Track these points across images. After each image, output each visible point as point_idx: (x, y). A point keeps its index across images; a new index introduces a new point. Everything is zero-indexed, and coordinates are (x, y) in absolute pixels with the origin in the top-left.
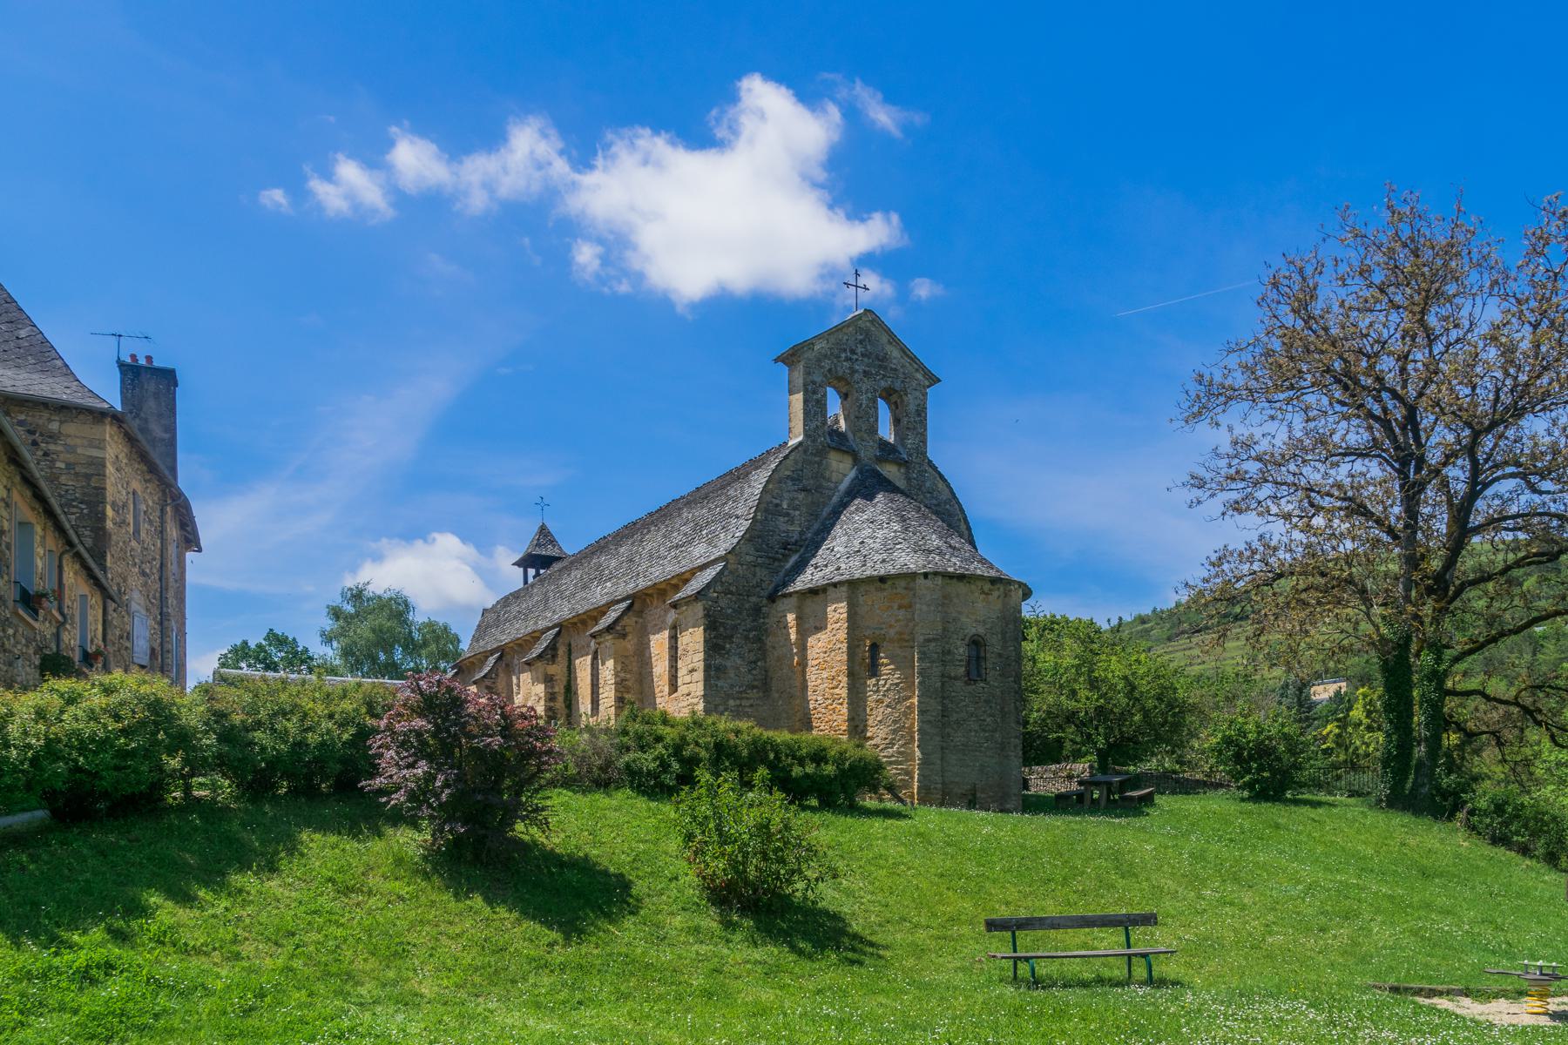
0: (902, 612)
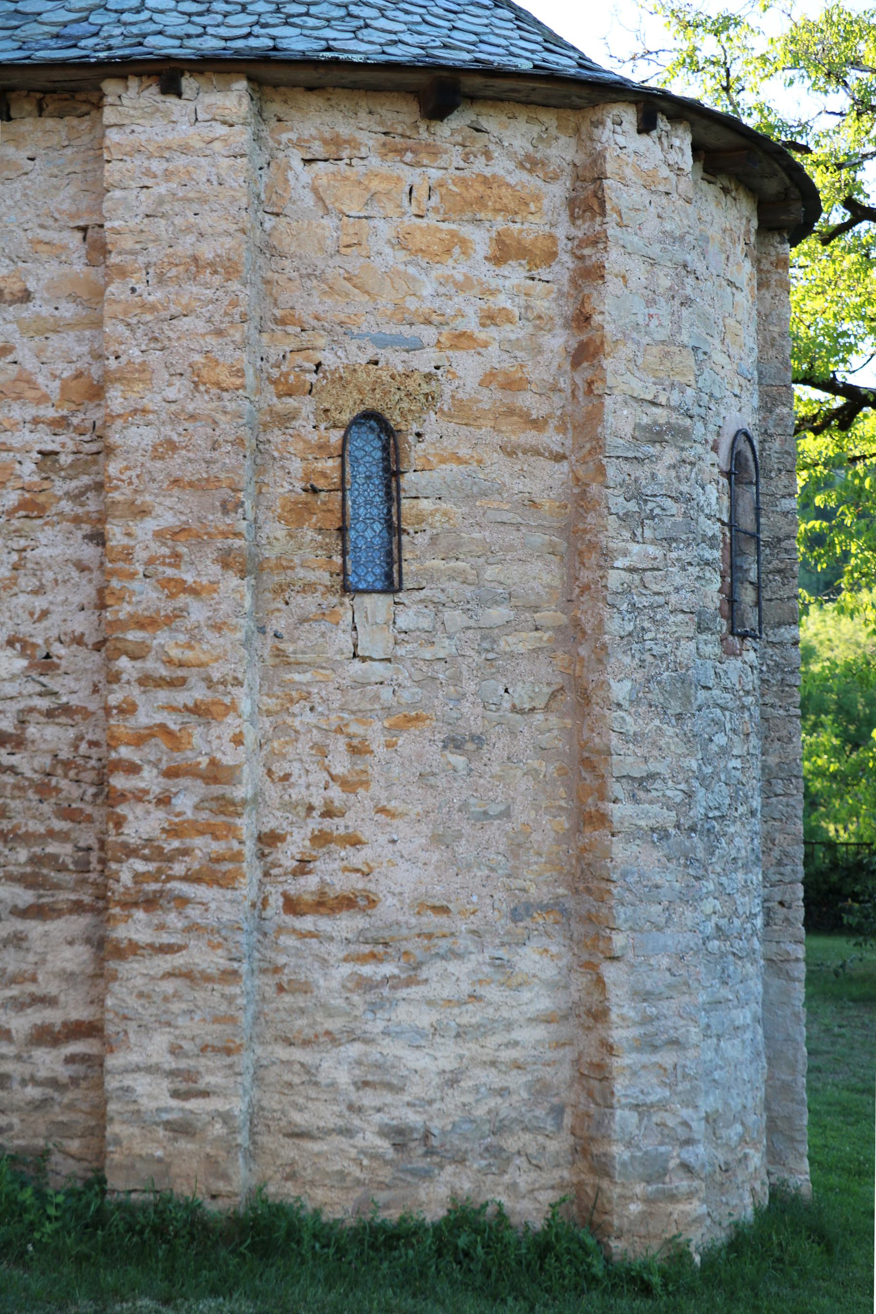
0: (514, 274)
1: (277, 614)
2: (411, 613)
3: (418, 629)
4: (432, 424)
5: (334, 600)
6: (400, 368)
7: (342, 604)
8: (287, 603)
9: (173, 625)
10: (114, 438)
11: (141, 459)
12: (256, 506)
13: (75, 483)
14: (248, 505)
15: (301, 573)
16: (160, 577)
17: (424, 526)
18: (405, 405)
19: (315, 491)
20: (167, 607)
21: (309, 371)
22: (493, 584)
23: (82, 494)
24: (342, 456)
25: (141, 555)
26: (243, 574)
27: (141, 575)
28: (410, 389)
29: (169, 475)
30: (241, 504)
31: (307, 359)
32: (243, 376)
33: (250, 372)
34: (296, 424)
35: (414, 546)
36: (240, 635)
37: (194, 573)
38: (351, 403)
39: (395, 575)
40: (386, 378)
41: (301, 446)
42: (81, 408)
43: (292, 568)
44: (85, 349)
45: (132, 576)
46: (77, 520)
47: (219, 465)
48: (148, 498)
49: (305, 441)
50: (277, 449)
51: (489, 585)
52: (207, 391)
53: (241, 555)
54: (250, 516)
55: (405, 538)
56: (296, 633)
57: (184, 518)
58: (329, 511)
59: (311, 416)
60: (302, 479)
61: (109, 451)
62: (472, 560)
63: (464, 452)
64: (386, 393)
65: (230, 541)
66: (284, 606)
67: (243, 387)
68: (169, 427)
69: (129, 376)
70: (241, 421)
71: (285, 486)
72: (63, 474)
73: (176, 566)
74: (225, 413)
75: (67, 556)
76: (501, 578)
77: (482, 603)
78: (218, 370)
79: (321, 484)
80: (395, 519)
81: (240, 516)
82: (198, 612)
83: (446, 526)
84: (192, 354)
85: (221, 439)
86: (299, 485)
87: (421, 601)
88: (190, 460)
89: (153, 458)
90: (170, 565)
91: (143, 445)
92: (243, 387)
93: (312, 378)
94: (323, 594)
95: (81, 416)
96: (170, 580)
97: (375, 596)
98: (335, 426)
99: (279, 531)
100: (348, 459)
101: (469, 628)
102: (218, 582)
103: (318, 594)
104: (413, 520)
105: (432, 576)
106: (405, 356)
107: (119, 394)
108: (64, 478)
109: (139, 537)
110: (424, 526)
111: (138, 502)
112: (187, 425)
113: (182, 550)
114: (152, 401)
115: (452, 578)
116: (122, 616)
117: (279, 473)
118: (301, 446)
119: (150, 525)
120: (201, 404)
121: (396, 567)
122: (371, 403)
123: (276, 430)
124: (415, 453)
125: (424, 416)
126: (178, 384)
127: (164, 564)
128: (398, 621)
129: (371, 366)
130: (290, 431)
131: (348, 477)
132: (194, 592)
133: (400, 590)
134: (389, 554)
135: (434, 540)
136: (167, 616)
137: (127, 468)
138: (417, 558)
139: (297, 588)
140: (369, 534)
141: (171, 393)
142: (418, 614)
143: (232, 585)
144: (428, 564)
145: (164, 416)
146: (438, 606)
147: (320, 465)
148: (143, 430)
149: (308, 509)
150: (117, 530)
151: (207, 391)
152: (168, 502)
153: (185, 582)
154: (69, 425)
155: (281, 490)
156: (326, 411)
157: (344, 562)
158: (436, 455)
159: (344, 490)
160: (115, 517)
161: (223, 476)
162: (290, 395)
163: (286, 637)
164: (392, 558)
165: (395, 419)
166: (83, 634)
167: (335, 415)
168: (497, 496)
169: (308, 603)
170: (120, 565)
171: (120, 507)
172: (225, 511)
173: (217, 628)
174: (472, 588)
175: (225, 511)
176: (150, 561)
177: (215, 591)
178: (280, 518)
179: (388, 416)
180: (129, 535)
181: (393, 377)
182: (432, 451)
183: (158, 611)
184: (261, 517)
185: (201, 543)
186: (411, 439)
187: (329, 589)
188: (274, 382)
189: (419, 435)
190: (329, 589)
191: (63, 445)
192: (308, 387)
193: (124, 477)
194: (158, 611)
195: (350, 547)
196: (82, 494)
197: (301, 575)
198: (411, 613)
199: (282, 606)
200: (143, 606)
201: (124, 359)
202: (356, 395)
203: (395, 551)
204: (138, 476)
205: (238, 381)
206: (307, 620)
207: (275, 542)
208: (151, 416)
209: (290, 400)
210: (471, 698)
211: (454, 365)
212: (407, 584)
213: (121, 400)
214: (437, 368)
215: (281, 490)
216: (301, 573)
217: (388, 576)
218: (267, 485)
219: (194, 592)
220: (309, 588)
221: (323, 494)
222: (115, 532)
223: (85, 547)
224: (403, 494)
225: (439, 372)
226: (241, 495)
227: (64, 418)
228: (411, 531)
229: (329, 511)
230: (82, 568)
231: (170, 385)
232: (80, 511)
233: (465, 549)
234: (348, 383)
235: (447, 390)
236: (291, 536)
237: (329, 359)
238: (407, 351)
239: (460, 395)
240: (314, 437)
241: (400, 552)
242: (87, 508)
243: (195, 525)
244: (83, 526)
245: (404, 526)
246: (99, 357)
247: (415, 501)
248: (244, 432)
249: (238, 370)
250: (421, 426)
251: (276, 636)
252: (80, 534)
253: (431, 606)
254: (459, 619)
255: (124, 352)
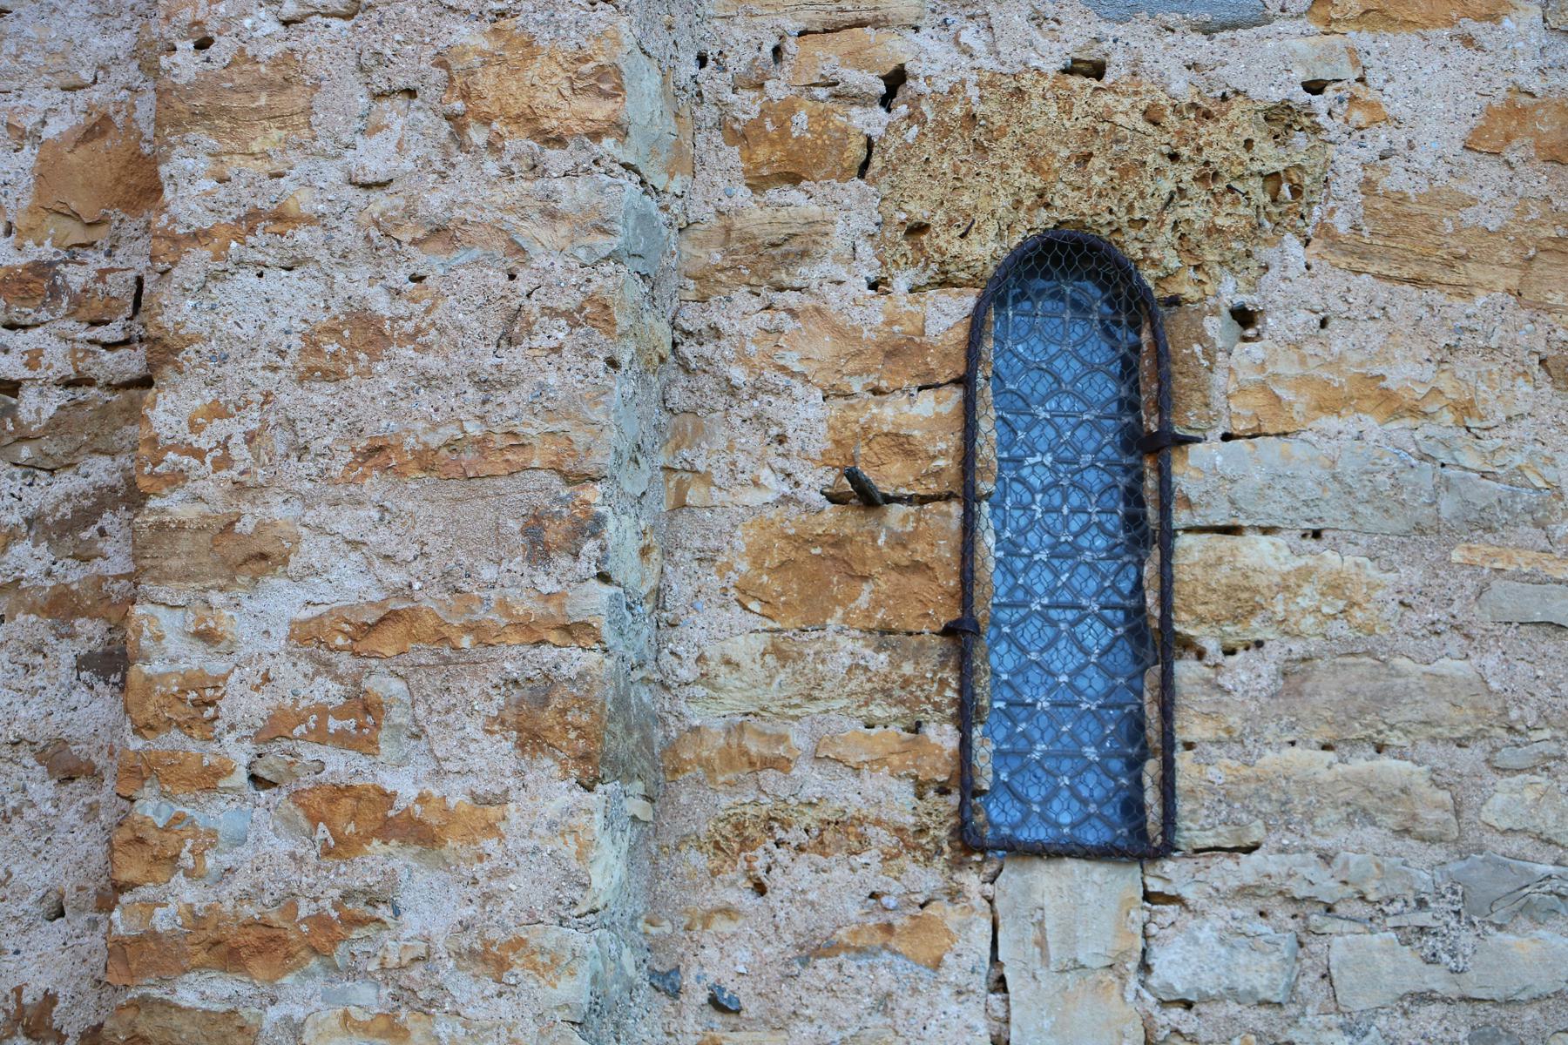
1: (722, 925)
2: (1206, 934)
3: (1233, 993)
4: (1292, 277)
5: (928, 878)
6: (1182, 87)
7: (954, 895)
8: (760, 889)
9: (340, 954)
10: (177, 311)
11: (265, 380)
12: (660, 546)
13: (67, 483)
14: (622, 531)
15: (812, 780)
16: (307, 781)
17: (1256, 627)
18: (1195, 211)
19: (866, 497)
20: (324, 888)
21: (858, 99)
22: (1515, 844)
23: (85, 517)
24: (965, 382)
25: (245, 705)
26: (590, 772)
27: (241, 777)
28: (1214, 155)
29: (355, 429)
30: (593, 526)
31: (857, 58)
32: (617, 92)
33: (645, 86)
34: (808, 273)
35: (1217, 702)
36: (572, 989)
37: (424, 766)
38: (1003, 202)
39: (1151, 797)
40: (1129, 119)
41: (825, 347)
42: (101, 235)
43: (780, 764)
44: (122, 42)
45: (209, 779)
46: (61, 607)
47: (524, 392)
48: (279, 511)
49: (839, 332)
50: (743, 359)
51: (1499, 846)
52: (493, 147)
53: (585, 703)
54: (627, 568)
55: (1186, 670)
56: (788, 997)
57: (396, 577)
58: (917, 567)
59: (865, 250)
60: (825, 460)
61: (163, 354)
62: (1438, 755)
63: (1406, 372)
64: (1128, 169)
65: (548, 654)
66: (749, 901)
67: (619, 129)
68: (362, 272)
69: (236, 102)
70: (603, 244)
71: (763, 485)
72: (25, 452)
73: (362, 743)
74: (552, 215)
75: (19, 728)
76: (1548, 821)
77: (1471, 908)
78: (533, 72)
79: (890, 476)
80: (1151, 599)
81: (586, 567)
82: (429, 906)
83: (1338, 628)
84: (448, 22)
85: (532, 306)
86: (815, 480)
87: (1245, 892)
88: (428, 380)
89: (305, 377)
90: (342, 740)
91: (272, 333)
92: (619, 129)
93: (872, 121)
94: (888, 858)
95: (97, 260)
96: (340, 791)
97: (1074, 868)
98: (945, 282)
99: (739, 636)
100: (986, 392)
101: (1425, 998)
102: (502, 799)
103: (871, 856)
104: (1217, 606)
105: (1286, 808)
106: (1198, 47)
107: (203, 164)
108: (31, 468)
109: (247, 644)
110: (1256, 627)
111: (246, 526)
112: (421, 260)
113: (385, 686)
114: (311, 186)
115: (1358, 815)
116: (162, 921)
117: (752, 439)
118: (825, 347)
119: (283, 601)
120: (475, 190)
121: (1152, 767)
122: (1072, 204)
123: (741, 296)
124: (1228, 376)
125: (1265, 253)
126: (398, 124)
127: (320, 736)
128: (1158, 959)
129: (1075, 81)
130: (791, 298)
131: (987, 451)
132: (419, 833)
133: (1167, 849)
134: (1137, 725)
135: (1294, 674)
136: (320, 921)
137: (217, 411)
138: (1229, 739)
139: (795, 836)
140: (1063, 660)
141: (373, 158)
142: (1231, 937)
143: (551, 810)
144: (1270, 760)
145: (347, 235)
146: (1310, 912)
147: (888, 413)
148: (275, 281)
149: (844, 561)
150: (168, 621)
151: (493, 147)
152: (346, 523)
153: (388, 798)
154: (55, 292)
155: (752, 497)
156: (917, 229)
157: (965, 745)
158: (1303, 381)
159: (969, 497)
160: (163, 578)
161: (532, 429)
162: (794, 179)
163: (752, 1008)
164: (1145, 740)
165: (1158, 257)
166: (50, 999)
167: (945, 241)
168: (1528, 532)
169: (831, 890)
170: (173, 739)
171: (184, 545)
172: (539, 551)
173: (492, 960)
174: (1438, 853)
175: (539, 551)
176: (274, 730)
177: (491, 829)
178: (745, 593)
179: (1134, 250)
180: (207, 636)
181: (1153, 117)
182: (1287, 367)
183: (288, 903)
184: (680, 589)
185: (451, 662)
186: (1217, 327)
187: (911, 840)
188: (741, 137)
189: (1244, 317)
190: (911, 840)
191: (34, 359)
192: (857, 151)
193: (202, 442)
194: (288, 903)
195: (990, 700)
196: (85, 517)
197: (811, 791)
198: (1206, 934)
199: (744, 898)
200: (239, 884)
201: (223, 49)
202: (1020, 176)
203: (1152, 713)
204: (250, 438)
205: (601, 110)
206: (830, 949)
207: (724, 675)
208: (302, 235)
209: (794, 195)
210: (507, 161)
211: (1376, 77)
212: (1194, 829)
213: (209, 184)
214: (1315, 87)
215: (752, 497)
216: (812, 780)
217: (1133, 808)
218: (706, 478)
219: (419, 833)
220: (839, 833)
221: (896, 511)
222: (166, 638)
223: (80, 696)
224: (1181, 517)
225: (1320, 103)
226: (593, 494)
227: (41, 269)
228: (1211, 645)
229: (917, 567)
230: (66, 767)
231: (370, 130)
232: (74, 575)
233: (1407, 713)
234: (995, 135)
235: (1348, 161)
236: (782, 656)
237: (932, 59)
238: (1208, 31)
239: (1395, 179)
240: (871, 316)
241: (1167, 714)
242: (98, 567)
243: (431, 600)
244: (84, 625)
245: (1184, 625)
246: (148, 57)
247: (1227, 541)
248: (620, 286)
249: (601, 72)
250: (1253, 285)
251: (715, 1003)
252: (67, 653)
253: (1281, 913)
254: (1385, 963)
255: (227, 22)
